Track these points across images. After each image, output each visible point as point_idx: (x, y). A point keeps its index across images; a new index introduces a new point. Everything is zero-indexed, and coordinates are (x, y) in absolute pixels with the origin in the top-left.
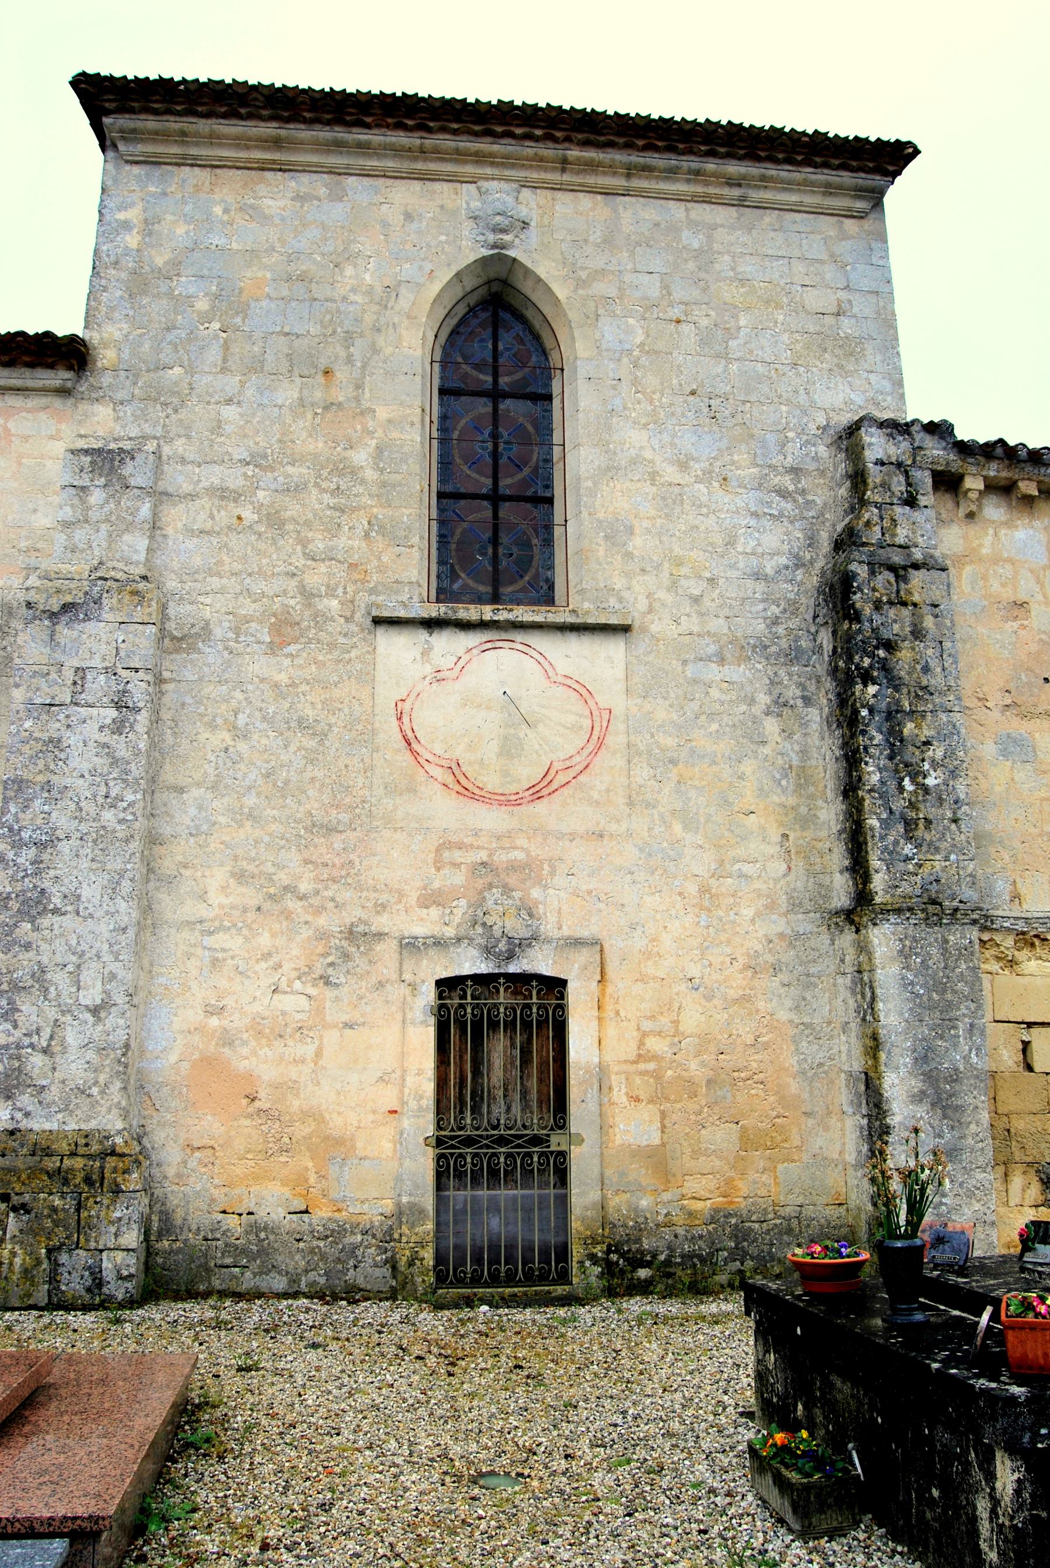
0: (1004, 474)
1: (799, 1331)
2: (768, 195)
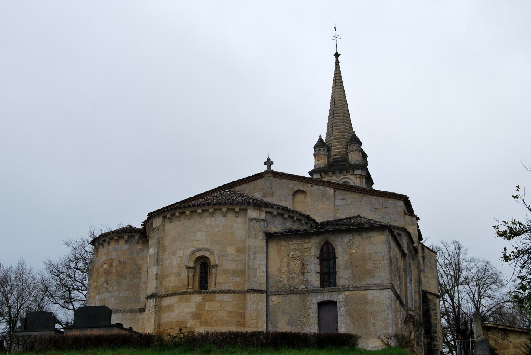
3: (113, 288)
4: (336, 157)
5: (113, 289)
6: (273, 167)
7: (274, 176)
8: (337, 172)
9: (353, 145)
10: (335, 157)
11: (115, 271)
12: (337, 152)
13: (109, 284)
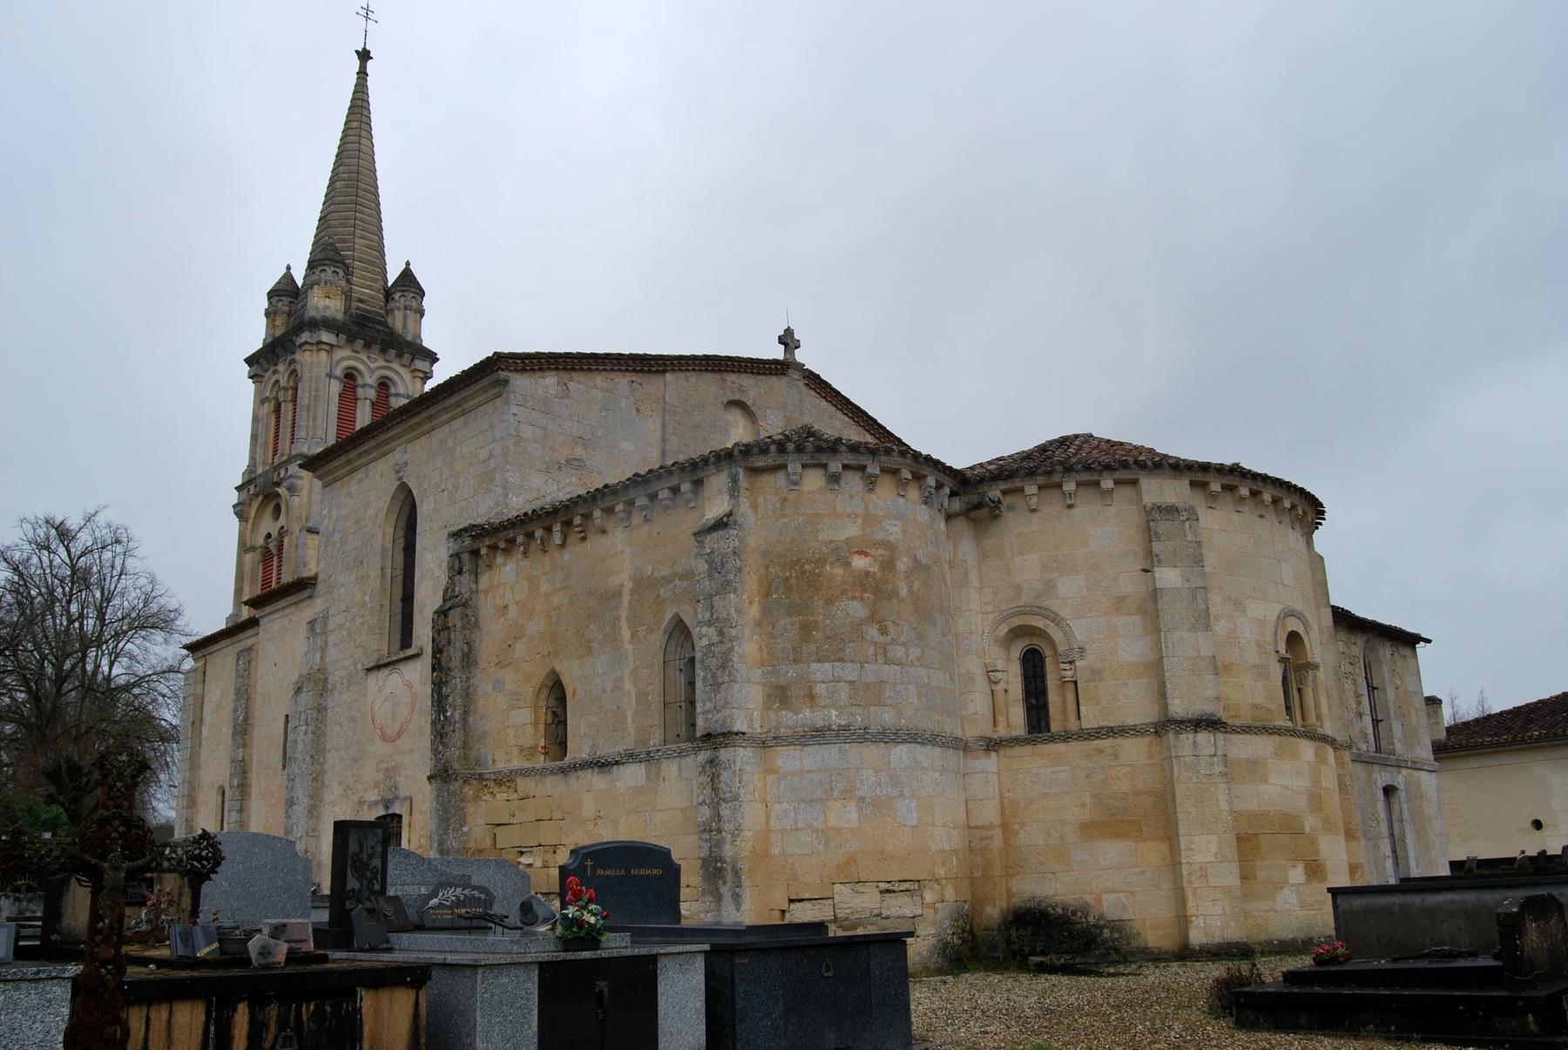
0: (492, 542)
1: (1461, 1008)
2: (470, 404)
3: (907, 649)
4: (364, 306)
5: (907, 654)
6: (800, 356)
7: (807, 382)
8: (376, 348)
9: (412, 295)
10: (361, 305)
11: (905, 590)
12: (365, 293)
13: (892, 634)
